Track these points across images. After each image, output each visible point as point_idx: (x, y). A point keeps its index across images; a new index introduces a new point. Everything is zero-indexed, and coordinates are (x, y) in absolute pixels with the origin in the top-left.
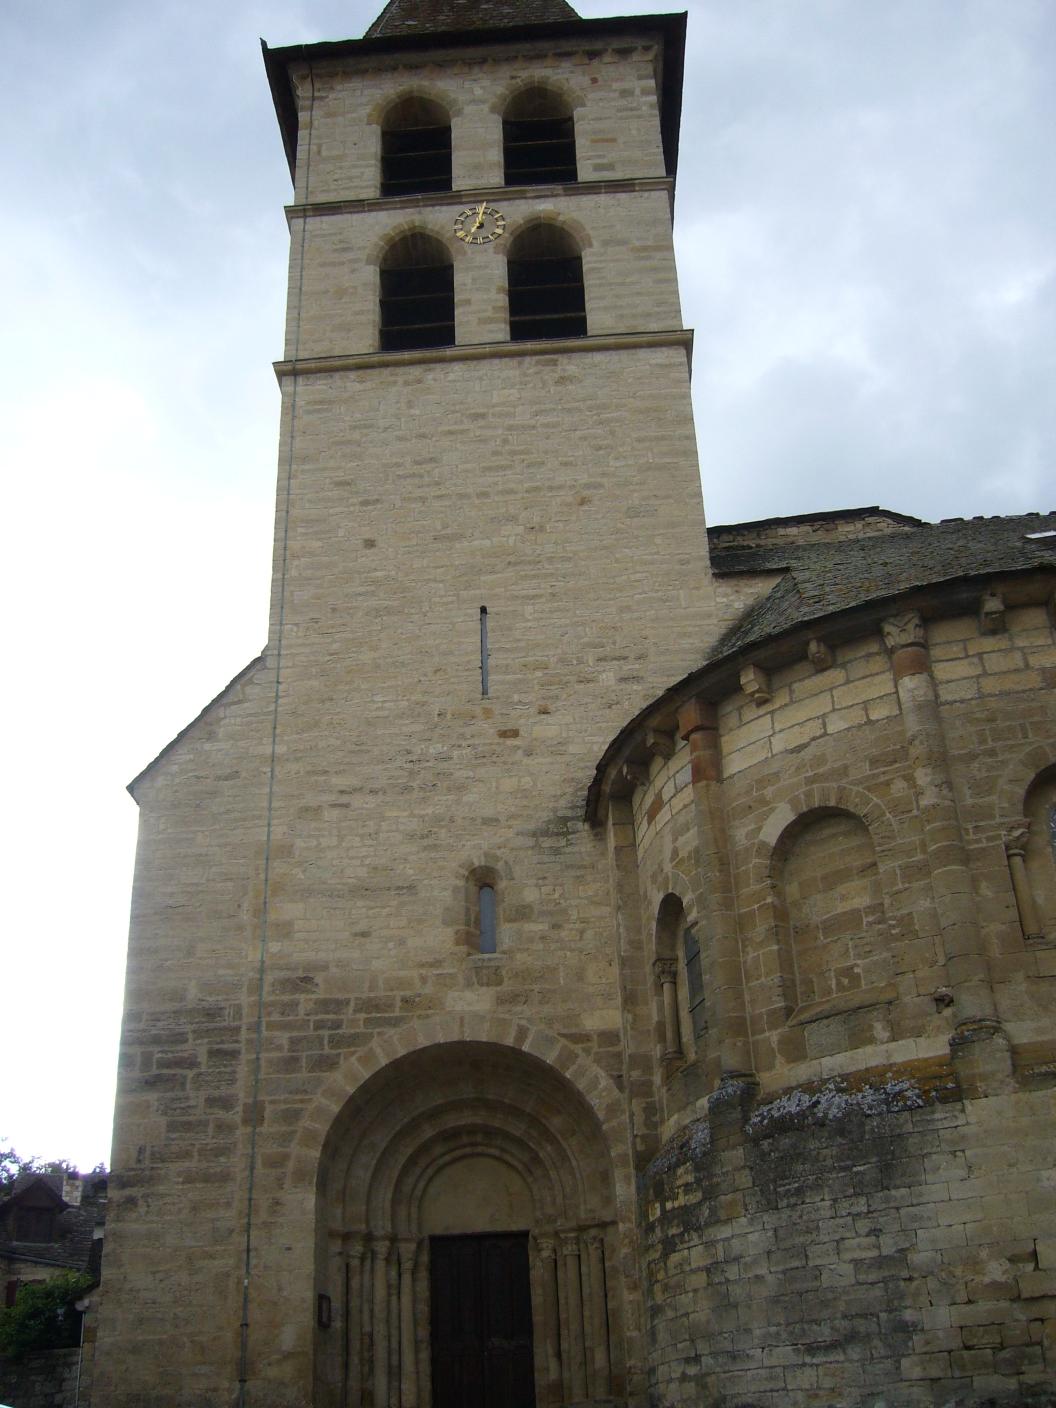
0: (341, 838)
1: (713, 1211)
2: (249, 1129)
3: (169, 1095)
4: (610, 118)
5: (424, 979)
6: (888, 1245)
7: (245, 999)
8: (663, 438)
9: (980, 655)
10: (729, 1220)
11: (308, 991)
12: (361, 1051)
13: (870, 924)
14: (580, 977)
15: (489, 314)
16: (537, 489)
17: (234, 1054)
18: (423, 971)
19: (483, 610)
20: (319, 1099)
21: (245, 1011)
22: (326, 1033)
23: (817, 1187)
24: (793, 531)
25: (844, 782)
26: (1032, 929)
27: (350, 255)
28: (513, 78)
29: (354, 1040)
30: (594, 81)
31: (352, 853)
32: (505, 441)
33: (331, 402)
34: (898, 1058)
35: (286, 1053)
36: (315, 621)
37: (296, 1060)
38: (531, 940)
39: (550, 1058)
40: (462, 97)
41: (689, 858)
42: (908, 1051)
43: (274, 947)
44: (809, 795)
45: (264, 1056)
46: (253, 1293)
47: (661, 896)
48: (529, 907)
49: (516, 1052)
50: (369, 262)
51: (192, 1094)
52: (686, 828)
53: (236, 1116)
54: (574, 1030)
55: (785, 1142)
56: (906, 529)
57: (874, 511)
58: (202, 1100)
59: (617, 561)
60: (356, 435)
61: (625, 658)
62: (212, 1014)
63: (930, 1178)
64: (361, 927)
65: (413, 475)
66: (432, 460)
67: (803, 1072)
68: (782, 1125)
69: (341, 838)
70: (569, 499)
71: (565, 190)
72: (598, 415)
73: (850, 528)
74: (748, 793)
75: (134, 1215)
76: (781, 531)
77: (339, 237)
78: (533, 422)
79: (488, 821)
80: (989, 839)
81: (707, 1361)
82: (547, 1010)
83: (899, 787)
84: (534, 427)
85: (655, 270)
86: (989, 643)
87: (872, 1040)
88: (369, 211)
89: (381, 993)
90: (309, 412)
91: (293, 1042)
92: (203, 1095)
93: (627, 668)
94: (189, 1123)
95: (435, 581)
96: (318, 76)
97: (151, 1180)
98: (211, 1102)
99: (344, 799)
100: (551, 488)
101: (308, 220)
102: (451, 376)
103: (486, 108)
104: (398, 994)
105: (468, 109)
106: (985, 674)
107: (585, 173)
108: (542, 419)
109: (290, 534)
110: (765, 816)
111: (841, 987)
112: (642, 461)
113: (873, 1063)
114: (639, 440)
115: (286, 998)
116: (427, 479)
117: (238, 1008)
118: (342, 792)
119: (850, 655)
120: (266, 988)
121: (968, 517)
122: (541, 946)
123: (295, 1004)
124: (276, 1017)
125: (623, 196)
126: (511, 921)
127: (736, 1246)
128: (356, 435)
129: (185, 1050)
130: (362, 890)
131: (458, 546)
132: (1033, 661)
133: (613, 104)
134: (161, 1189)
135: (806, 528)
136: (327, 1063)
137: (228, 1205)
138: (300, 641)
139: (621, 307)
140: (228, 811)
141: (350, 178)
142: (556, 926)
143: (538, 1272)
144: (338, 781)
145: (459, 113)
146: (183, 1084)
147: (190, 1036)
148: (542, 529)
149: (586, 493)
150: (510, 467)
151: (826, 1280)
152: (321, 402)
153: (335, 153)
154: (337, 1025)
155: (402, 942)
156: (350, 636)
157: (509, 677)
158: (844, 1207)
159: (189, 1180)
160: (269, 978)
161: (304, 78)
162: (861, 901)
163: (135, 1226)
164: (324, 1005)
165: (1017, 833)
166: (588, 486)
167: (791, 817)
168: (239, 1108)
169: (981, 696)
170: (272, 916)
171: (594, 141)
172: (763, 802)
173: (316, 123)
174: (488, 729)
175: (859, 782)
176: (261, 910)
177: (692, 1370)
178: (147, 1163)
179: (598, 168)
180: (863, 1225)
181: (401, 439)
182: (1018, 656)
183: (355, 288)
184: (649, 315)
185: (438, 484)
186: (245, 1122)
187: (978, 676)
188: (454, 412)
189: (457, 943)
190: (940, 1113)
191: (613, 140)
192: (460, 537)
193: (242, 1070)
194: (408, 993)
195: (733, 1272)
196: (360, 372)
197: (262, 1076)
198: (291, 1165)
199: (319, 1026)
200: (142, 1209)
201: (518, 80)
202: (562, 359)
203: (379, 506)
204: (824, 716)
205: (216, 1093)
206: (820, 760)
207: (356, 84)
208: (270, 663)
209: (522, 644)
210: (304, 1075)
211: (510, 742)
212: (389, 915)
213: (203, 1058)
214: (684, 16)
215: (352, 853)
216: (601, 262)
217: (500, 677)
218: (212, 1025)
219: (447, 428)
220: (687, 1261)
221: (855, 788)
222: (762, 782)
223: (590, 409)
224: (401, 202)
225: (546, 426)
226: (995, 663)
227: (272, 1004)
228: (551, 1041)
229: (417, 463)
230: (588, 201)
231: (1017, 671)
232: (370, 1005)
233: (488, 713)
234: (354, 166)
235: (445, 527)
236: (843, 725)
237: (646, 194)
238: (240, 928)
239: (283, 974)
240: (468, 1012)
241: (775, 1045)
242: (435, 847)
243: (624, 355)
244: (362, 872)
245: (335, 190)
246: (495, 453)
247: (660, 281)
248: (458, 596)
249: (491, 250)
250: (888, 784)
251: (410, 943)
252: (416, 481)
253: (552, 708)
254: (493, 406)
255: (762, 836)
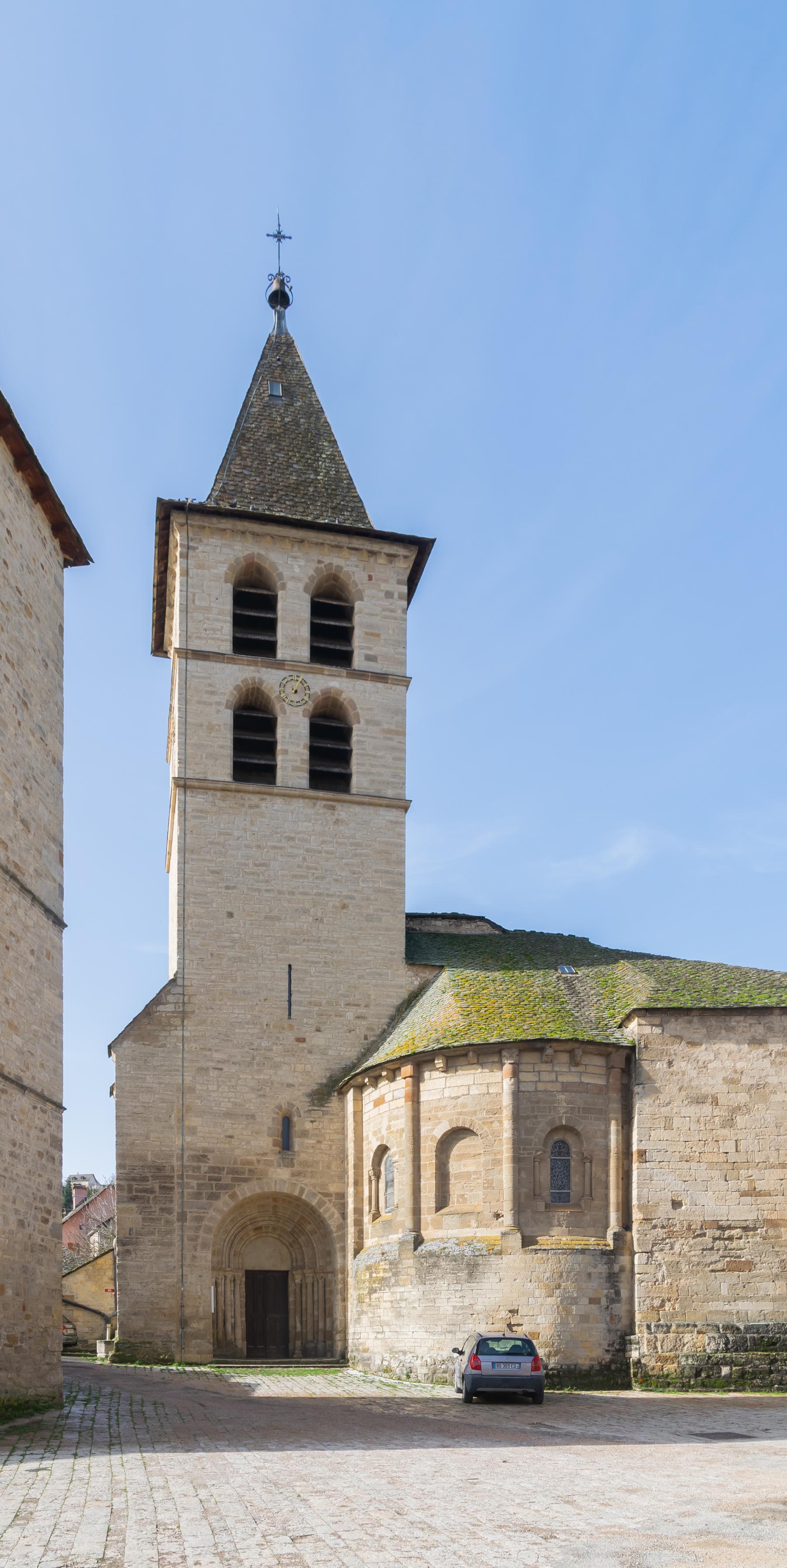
0: (219, 1087)
1: (397, 1281)
2: (180, 1224)
3: (143, 1205)
4: (377, 615)
5: (258, 1161)
6: (467, 1302)
7: (176, 1163)
8: (388, 872)
9: (539, 1072)
10: (404, 1285)
11: (203, 1162)
12: (230, 1192)
13: (474, 1179)
14: (329, 1167)
15: (298, 764)
16: (320, 894)
17: (172, 1189)
18: (259, 1158)
19: (290, 966)
20: (212, 1213)
21: (176, 1168)
22: (214, 1183)
23: (443, 1278)
24: (439, 923)
25: (473, 1118)
26: (537, 1192)
27: (216, 698)
28: (320, 562)
29: (226, 1187)
30: (370, 578)
31: (224, 1095)
32: (304, 859)
33: (207, 812)
34: (479, 1235)
35: (195, 1190)
36: (202, 959)
37: (201, 1194)
38: (308, 1148)
39: (314, 1203)
40: (286, 573)
41: (397, 1132)
42: (482, 1233)
43: (188, 1139)
44: (457, 1120)
45: (185, 1191)
46: (186, 1294)
47: (379, 1143)
48: (307, 1131)
49: (298, 1199)
50: (227, 707)
51: (153, 1206)
52: (397, 1118)
53: (174, 1217)
54: (325, 1191)
55: (431, 1261)
56: (497, 932)
57: (482, 919)
58: (158, 1209)
59: (359, 947)
60: (221, 839)
61: (359, 1005)
62: (160, 1169)
63: (486, 1281)
64: (230, 1133)
65: (253, 873)
66: (263, 865)
67: (440, 1233)
68: (431, 1254)
69: (219, 1087)
70: (337, 904)
71: (347, 673)
72: (355, 850)
73: (468, 926)
74: (430, 1111)
75: (130, 1258)
76: (433, 922)
77: (209, 681)
78: (319, 848)
79: (290, 1085)
80: (528, 1154)
81: (388, 1334)
82: (313, 1181)
83: (496, 1125)
84: (320, 852)
85: (393, 749)
86: (544, 1067)
87: (469, 1226)
88: (228, 663)
89: (239, 1166)
90: (195, 817)
91: (199, 1185)
92: (158, 1206)
93: (362, 1011)
94: (152, 1219)
95: (265, 945)
96: (192, 526)
97: (136, 1243)
98: (162, 1210)
99: (220, 1066)
100: (328, 895)
101: (189, 661)
102: (276, 807)
103: (301, 586)
104: (247, 1167)
105: (290, 585)
106: (540, 1081)
107: (358, 662)
108: (326, 848)
109: (186, 901)
110: (437, 1124)
111: (458, 1202)
112: (376, 885)
113: (469, 1235)
114: (376, 871)
115: (195, 1164)
116: (261, 877)
117: (173, 1168)
118: (219, 1061)
119: (485, 1061)
120: (185, 1158)
121: (528, 930)
122: (312, 1151)
123: (199, 1168)
124: (190, 1173)
125: (380, 685)
126: (299, 1137)
127: (406, 1295)
128: (221, 839)
129: (149, 1185)
130: (228, 1115)
131: (277, 924)
132: (560, 1079)
133: (380, 602)
134: (142, 1247)
135: (446, 922)
136: (214, 1197)
137: (172, 1256)
138: (194, 971)
139: (373, 774)
140: (162, 1066)
141: (214, 630)
142: (319, 1142)
143: (291, 1287)
144: (217, 1056)
145: (284, 587)
146: (148, 1200)
147: (150, 1179)
148: (322, 921)
149: (347, 901)
150: (307, 877)
151: (441, 1311)
152: (201, 811)
153: (205, 604)
154: (219, 1179)
155: (248, 1143)
156: (220, 972)
157: (302, 1008)
158: (452, 1287)
159: (154, 1244)
160: (186, 1154)
161: (182, 525)
162: (472, 1169)
163: (130, 1263)
164: (213, 1169)
165: (539, 1153)
166: (347, 897)
167: (448, 1128)
168: (175, 1214)
169: (536, 1091)
170: (186, 1123)
171: (366, 634)
172: (436, 1117)
173: (190, 572)
174: (290, 1036)
175: (480, 1120)
176: (182, 1120)
177: (380, 1336)
178: (134, 1235)
179: (369, 658)
180: (458, 1294)
181: (246, 846)
182: (554, 1075)
183: (219, 726)
184: (388, 783)
185: (267, 881)
186: (178, 1220)
187: (536, 1082)
188: (277, 833)
189: (274, 1145)
190: (493, 1258)
191: (378, 635)
192: (278, 919)
193: (176, 1197)
194: (251, 1167)
195: (403, 1304)
196: (224, 793)
197: (185, 1200)
198: (200, 1240)
199: (210, 1179)
200: (134, 1256)
201: (322, 565)
202: (338, 806)
203: (235, 891)
204: (469, 1086)
205: (164, 1206)
206: (464, 1106)
207: (215, 540)
208: (180, 982)
209: (309, 990)
210: (204, 1201)
211: (301, 1045)
212: (243, 1128)
213: (157, 1189)
214: (433, 541)
215: (224, 1095)
216: (365, 736)
217: (298, 1008)
218: (160, 1174)
219: (274, 844)
220: (382, 1297)
221: (478, 1122)
222: (437, 1109)
223: (352, 844)
224: (248, 661)
225: (327, 852)
226: (545, 1077)
227: (189, 1166)
228: (314, 1195)
229: (256, 865)
230: (360, 684)
231: (552, 1082)
232: (233, 1171)
233: (291, 1027)
234: (217, 620)
235: (271, 911)
236: (477, 1092)
237: (394, 687)
238: (171, 1128)
239: (192, 1153)
240: (279, 1178)
241: (429, 1221)
242: (264, 1096)
243: (371, 810)
244: (230, 1105)
245: (205, 638)
246: (299, 866)
247: (395, 759)
248: (276, 955)
249: (301, 713)
250: (492, 1122)
251: (252, 1143)
252: (256, 877)
253: (323, 1028)
254: (300, 833)
255: (434, 1133)
